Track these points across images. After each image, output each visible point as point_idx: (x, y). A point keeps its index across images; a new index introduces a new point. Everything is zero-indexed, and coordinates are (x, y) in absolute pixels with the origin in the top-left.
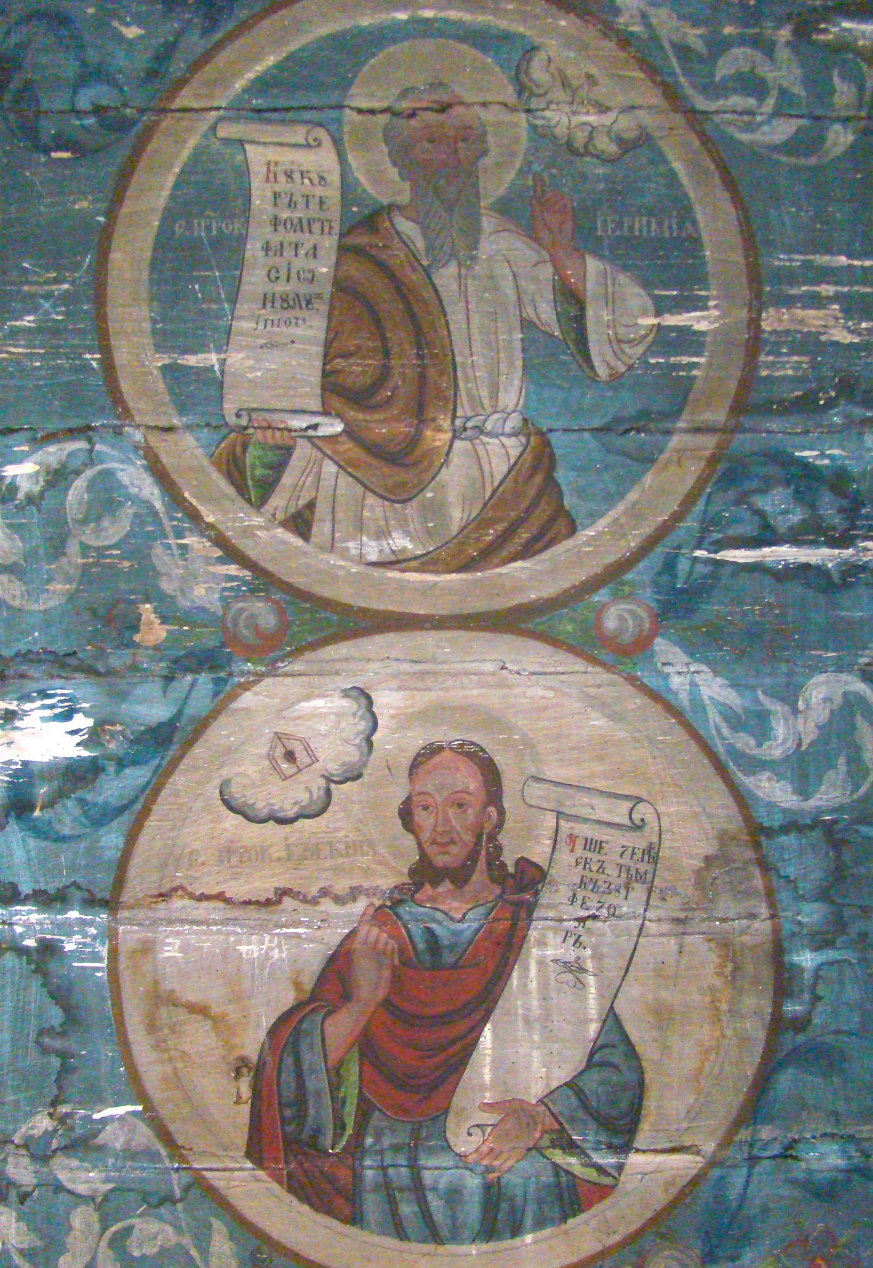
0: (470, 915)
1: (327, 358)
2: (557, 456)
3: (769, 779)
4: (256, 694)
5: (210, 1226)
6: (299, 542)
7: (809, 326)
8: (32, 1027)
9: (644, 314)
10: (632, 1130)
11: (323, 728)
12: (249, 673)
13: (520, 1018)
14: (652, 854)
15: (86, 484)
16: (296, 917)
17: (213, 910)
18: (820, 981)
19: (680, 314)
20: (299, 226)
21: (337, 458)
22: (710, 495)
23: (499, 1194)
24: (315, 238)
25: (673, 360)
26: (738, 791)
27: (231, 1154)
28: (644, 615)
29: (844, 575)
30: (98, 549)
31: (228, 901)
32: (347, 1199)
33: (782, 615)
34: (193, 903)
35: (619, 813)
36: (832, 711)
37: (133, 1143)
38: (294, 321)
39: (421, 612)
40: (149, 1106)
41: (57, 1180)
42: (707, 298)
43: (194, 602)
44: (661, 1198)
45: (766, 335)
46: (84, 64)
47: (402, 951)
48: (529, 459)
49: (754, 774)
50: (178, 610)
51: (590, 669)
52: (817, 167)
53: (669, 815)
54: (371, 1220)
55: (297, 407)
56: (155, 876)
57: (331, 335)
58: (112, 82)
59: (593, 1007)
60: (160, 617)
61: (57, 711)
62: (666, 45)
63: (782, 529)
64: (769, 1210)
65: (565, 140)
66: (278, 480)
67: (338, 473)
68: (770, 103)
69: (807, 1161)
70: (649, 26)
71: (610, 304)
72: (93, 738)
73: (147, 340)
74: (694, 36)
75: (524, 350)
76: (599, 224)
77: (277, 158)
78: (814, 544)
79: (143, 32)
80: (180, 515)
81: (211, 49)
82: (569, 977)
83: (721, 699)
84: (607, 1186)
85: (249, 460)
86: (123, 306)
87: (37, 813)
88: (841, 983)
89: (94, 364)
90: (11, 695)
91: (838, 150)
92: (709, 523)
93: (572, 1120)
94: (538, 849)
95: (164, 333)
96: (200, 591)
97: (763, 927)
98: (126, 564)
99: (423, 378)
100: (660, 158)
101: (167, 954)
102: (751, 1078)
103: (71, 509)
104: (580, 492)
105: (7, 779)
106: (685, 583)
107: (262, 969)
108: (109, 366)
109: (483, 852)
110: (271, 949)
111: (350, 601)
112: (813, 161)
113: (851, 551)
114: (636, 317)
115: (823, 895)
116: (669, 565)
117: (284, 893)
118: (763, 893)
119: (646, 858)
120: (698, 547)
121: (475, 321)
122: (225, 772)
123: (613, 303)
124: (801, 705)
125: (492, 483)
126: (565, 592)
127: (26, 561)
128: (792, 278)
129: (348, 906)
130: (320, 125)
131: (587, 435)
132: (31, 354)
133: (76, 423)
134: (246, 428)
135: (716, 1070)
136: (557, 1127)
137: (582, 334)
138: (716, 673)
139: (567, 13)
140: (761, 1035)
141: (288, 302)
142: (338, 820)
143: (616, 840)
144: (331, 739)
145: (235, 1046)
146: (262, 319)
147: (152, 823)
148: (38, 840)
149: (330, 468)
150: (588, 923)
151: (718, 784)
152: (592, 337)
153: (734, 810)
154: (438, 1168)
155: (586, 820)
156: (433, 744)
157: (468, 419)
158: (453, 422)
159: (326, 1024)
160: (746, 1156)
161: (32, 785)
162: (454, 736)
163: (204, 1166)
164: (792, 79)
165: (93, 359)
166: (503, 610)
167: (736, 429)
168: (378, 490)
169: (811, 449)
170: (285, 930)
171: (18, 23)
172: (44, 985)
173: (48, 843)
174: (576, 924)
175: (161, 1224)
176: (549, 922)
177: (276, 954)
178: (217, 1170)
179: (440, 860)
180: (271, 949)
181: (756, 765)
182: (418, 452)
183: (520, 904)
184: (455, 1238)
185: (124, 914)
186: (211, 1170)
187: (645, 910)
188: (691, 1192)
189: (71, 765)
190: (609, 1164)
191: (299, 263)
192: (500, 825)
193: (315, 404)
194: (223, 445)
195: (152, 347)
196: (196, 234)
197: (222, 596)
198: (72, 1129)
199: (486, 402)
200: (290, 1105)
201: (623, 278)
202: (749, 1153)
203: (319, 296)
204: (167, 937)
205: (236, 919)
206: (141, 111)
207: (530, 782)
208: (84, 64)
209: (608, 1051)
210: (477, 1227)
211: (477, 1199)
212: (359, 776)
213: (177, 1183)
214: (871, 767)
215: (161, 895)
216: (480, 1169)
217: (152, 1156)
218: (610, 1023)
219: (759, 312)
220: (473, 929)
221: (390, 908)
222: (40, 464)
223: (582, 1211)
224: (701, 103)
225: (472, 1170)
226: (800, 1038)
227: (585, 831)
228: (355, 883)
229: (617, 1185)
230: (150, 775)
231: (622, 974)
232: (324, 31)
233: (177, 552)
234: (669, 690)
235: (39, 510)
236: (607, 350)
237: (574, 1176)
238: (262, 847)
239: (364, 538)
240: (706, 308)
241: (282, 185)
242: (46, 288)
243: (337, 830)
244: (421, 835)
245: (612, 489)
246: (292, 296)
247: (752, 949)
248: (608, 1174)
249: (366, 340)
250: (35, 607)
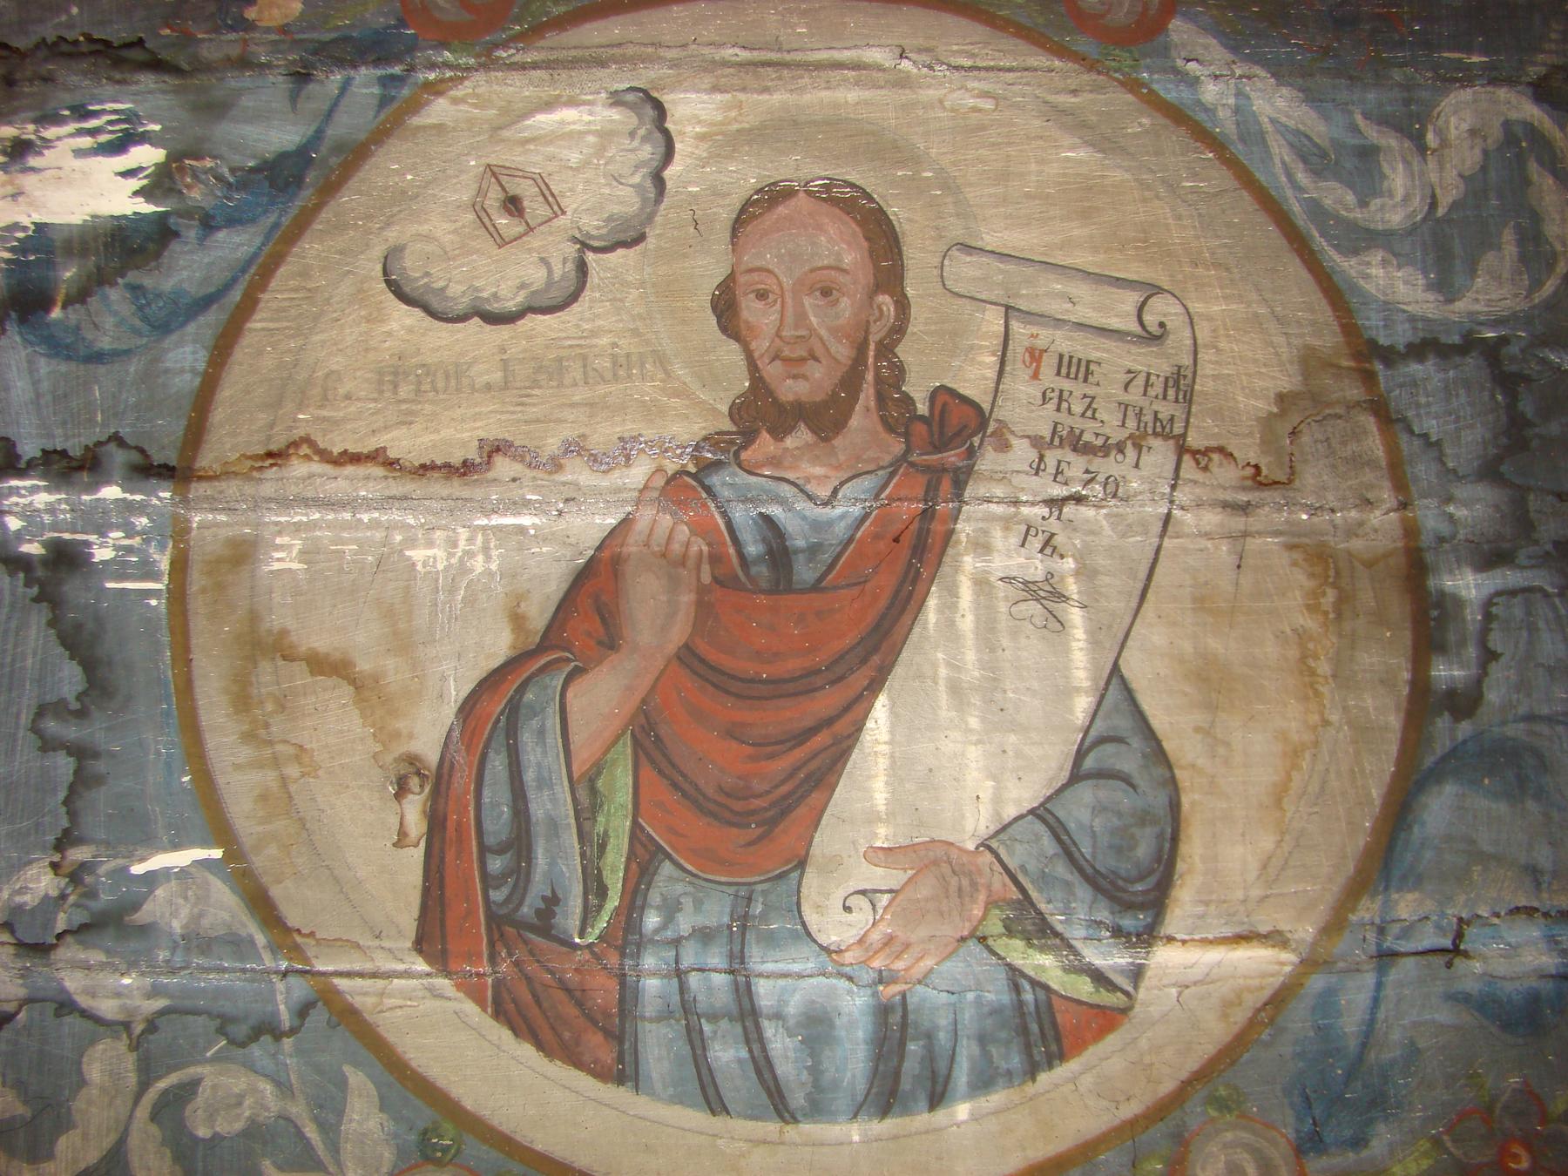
0: (846, 490)
3: (1384, 263)
4: (455, 101)
5: (342, 1084)
8: (25, 701)
10: (1157, 901)
11: (574, 158)
12: (447, 65)
13: (942, 686)
14: (1181, 385)
16: (516, 493)
17: (366, 483)
18: (1494, 625)
23: (904, 1024)
26: (1329, 278)
27: (386, 944)
31: (391, 464)
32: (607, 1033)
34: (328, 469)
35: (1120, 311)
36: (1485, 152)
37: (205, 922)
40: (235, 853)
41: (63, 990)
44: (1215, 1033)
47: (716, 559)
49: (1355, 252)
51: (1057, 63)
53: (1210, 318)
54: (655, 1075)
56: (263, 418)
59: (1081, 665)
61: (103, 138)
64: (1419, 1051)
69: (1484, 959)
72: (160, 184)
82: (1034, 608)
83: (1291, 124)
84: (1113, 1009)
87: (56, 313)
88: (1532, 629)
90: (23, 115)
93: (1044, 880)
94: (972, 372)
97: (1383, 520)
101: (276, 566)
102: (1378, 802)
105: (7, 255)
107: (452, 590)
109: (870, 377)
110: (469, 554)
115: (1490, 472)
117: (495, 449)
118: (1383, 463)
119: (1171, 393)
122: (393, 235)
124: (1431, 139)
129: (616, 473)
135: (1314, 787)
136: (1015, 894)
140: (1394, 721)
142: (598, 316)
143: (1115, 360)
144: (589, 174)
145: (396, 735)
147: (259, 325)
148: (54, 362)
150: (1069, 510)
151: (1294, 267)
153: (1325, 312)
154: (785, 975)
155: (1059, 323)
156: (774, 184)
159: (570, 694)
160: (1373, 949)
161: (50, 264)
162: (815, 171)
163: (344, 966)
170: (496, 520)
172: (52, 624)
173: (73, 365)
174: (1045, 511)
175: (253, 1077)
176: (993, 507)
177: (478, 564)
178: (361, 975)
179: (790, 390)
180: (469, 554)
181: (1361, 239)
183: (936, 472)
184: (818, 1109)
185: (198, 490)
186: (348, 975)
187: (1173, 487)
188: (1272, 1020)
189: (120, 228)
190: (1113, 968)
192: (899, 330)
198: (92, 894)
200: (500, 851)
202: (1378, 945)
204: (280, 533)
205: (405, 498)
207: (954, 252)
209: (1109, 748)
210: (861, 1086)
211: (860, 1034)
212: (641, 238)
213: (284, 999)
214: (1559, 247)
215: (270, 455)
216: (867, 976)
217: (238, 945)
218: (1114, 693)
220: (849, 521)
221: (693, 476)
223: (1062, 1057)
225: (850, 979)
226: (1465, 728)
227: (1064, 342)
228: (629, 428)
229: (1130, 1008)
230: (258, 241)
231: (1134, 604)
234: (1199, 102)
237: (1046, 988)
238: (457, 365)
243: (594, 334)
244: (753, 345)
247: (1369, 564)
248: (1111, 986)
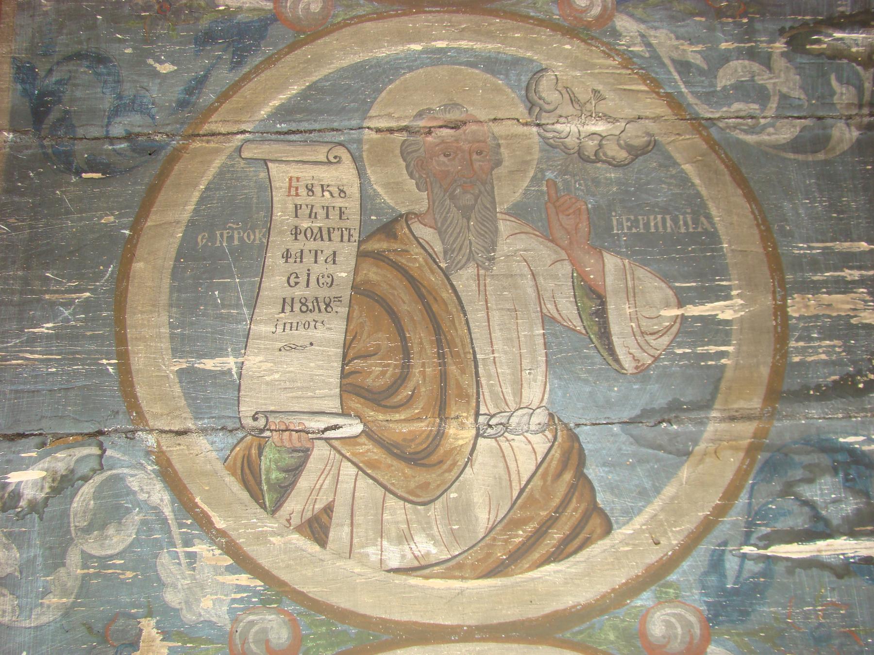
1: (346, 359)
2: (586, 452)
6: (317, 548)
7: (838, 310)
9: (668, 306)
15: (92, 490)
19: (703, 304)
20: (319, 235)
21: (355, 460)
22: (753, 485)
24: (336, 245)
25: (700, 350)
28: (692, 619)
30: (99, 558)
33: (850, 615)
38: (312, 324)
39: (448, 623)
42: (729, 288)
43: (200, 615)
45: (794, 321)
46: (120, 97)
48: (557, 455)
50: (183, 624)
52: (826, 162)
55: (316, 408)
57: (349, 338)
58: (143, 110)
60: (163, 633)
62: (667, 61)
63: (835, 522)
65: (577, 148)
66: (293, 484)
67: (357, 475)
68: (773, 105)
70: (649, 45)
71: (631, 299)
73: (165, 345)
74: (693, 53)
75: (546, 345)
76: (615, 223)
77: (300, 175)
79: (176, 68)
80: (189, 522)
81: (239, 81)
85: (264, 464)
86: (142, 313)
89: (111, 369)
91: (846, 146)
92: (754, 517)
95: (183, 336)
96: (206, 605)
98: (129, 574)
99: (444, 376)
100: (669, 161)
103: (75, 515)
104: (612, 488)
106: (735, 583)
108: (125, 369)
111: (368, 612)
112: (821, 156)
114: (659, 310)
116: (716, 564)
120: (746, 543)
121: (495, 316)
123: (634, 297)
125: (520, 481)
126: (604, 596)
127: (21, 573)
128: (815, 265)
130: (340, 144)
131: (616, 428)
132: (46, 359)
133: (92, 428)
134: (262, 431)
137: (605, 328)
139: (572, 38)
141: (305, 306)
146: (281, 323)
149: (348, 470)
152: (614, 328)
157: (492, 416)
158: (476, 420)
164: (791, 85)
165: (109, 364)
166: (537, 619)
167: (773, 415)
168: (400, 492)
169: (856, 435)
171: (58, 63)
182: (441, 451)
191: (317, 269)
193: (334, 405)
194: (238, 449)
195: (170, 351)
196: (218, 244)
197: (231, 608)
199: (510, 398)
201: (641, 272)
203: (338, 299)
206: (171, 136)
208: (120, 97)
219: (784, 299)
222: (47, 470)
224: (705, 111)
232: (346, 62)
233: (184, 561)
235: (41, 519)
236: (631, 341)
239: (385, 543)
240: (728, 297)
241: (303, 198)
242: (67, 296)
245: (648, 484)
246: (311, 299)
249: (384, 340)
250: (26, 624)
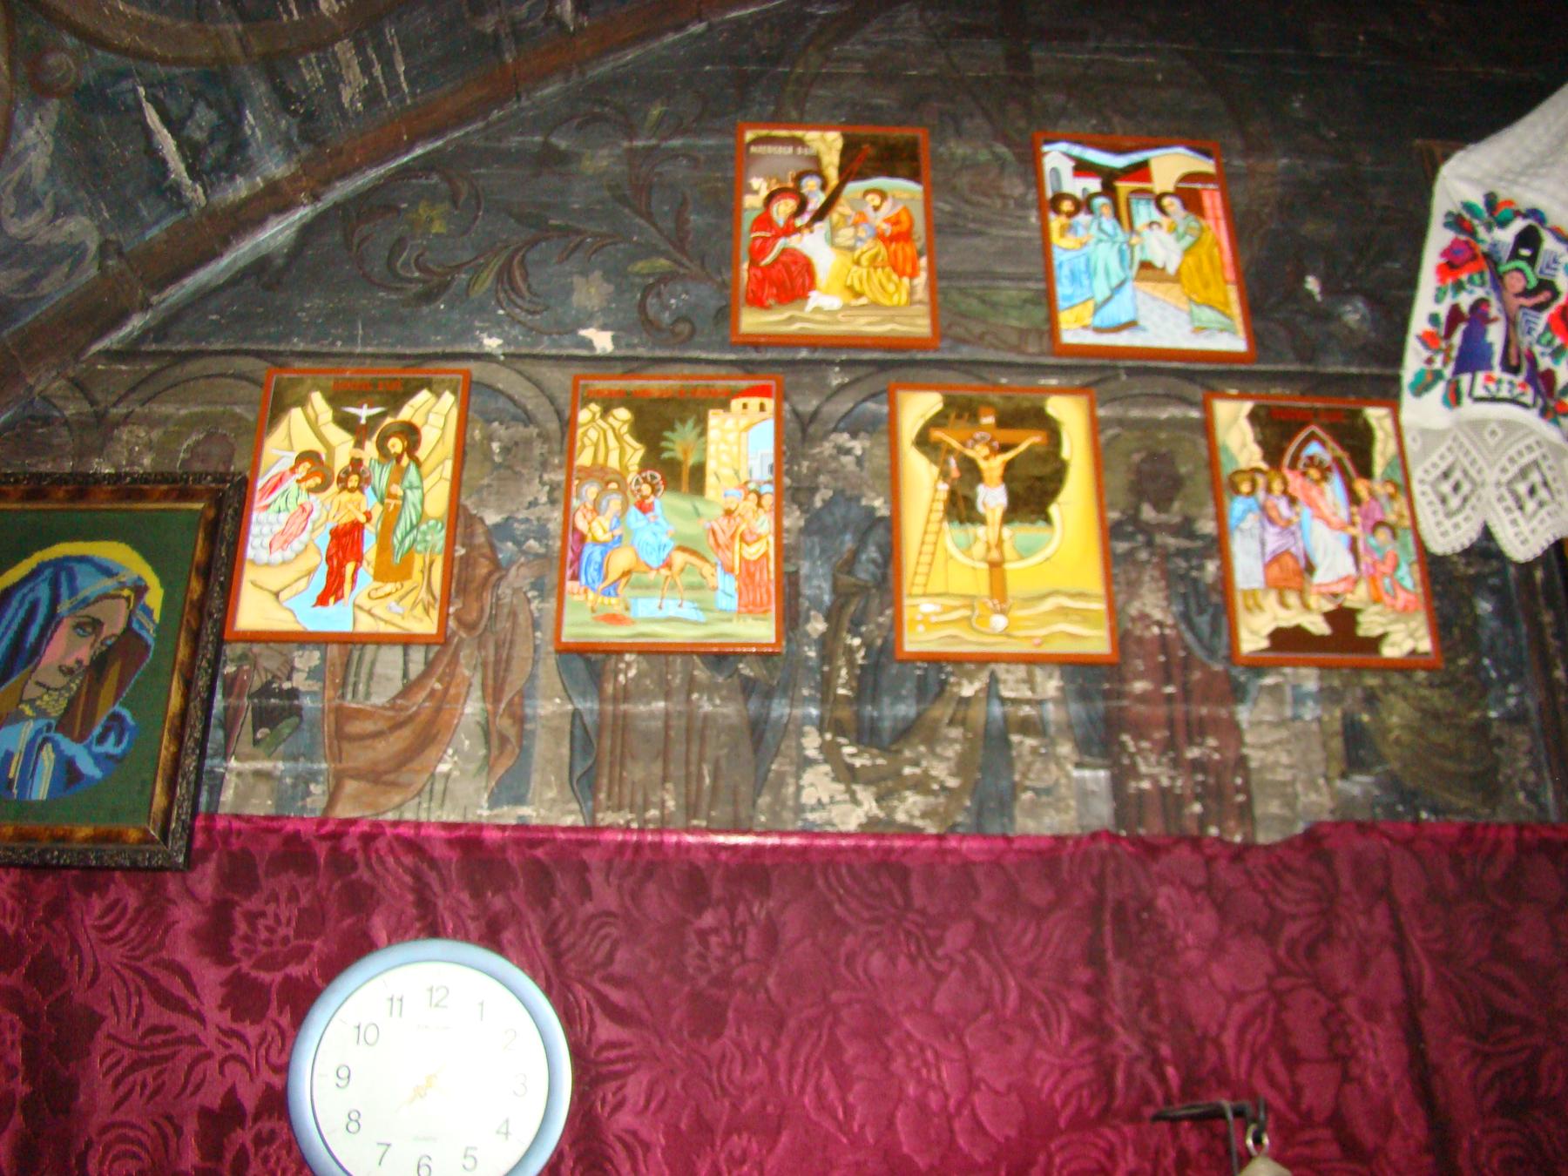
29: (170, 188)
63: (185, 133)
78: (184, 158)
92: (170, 84)
113: (189, 182)
120: (146, 87)
124: (59, 222)
138: (52, 156)
